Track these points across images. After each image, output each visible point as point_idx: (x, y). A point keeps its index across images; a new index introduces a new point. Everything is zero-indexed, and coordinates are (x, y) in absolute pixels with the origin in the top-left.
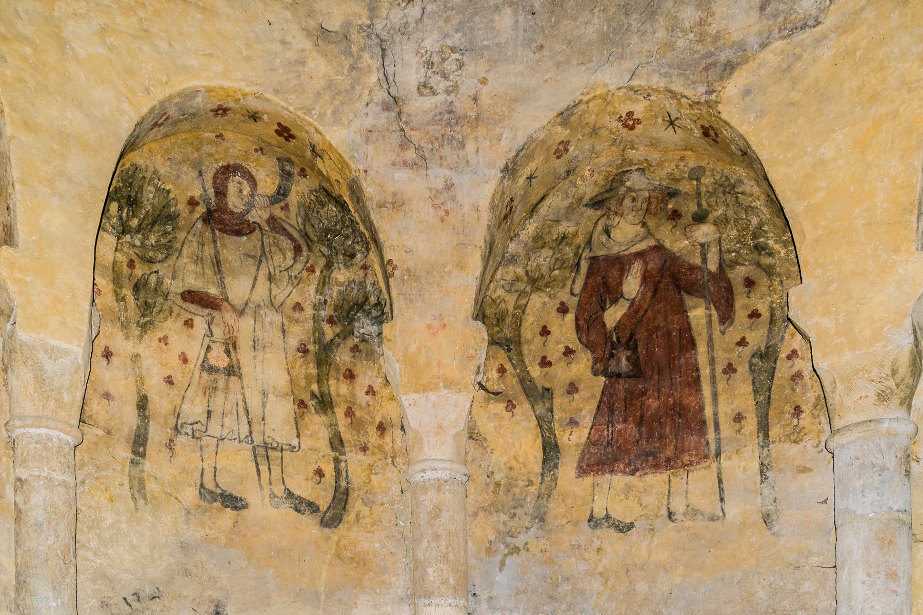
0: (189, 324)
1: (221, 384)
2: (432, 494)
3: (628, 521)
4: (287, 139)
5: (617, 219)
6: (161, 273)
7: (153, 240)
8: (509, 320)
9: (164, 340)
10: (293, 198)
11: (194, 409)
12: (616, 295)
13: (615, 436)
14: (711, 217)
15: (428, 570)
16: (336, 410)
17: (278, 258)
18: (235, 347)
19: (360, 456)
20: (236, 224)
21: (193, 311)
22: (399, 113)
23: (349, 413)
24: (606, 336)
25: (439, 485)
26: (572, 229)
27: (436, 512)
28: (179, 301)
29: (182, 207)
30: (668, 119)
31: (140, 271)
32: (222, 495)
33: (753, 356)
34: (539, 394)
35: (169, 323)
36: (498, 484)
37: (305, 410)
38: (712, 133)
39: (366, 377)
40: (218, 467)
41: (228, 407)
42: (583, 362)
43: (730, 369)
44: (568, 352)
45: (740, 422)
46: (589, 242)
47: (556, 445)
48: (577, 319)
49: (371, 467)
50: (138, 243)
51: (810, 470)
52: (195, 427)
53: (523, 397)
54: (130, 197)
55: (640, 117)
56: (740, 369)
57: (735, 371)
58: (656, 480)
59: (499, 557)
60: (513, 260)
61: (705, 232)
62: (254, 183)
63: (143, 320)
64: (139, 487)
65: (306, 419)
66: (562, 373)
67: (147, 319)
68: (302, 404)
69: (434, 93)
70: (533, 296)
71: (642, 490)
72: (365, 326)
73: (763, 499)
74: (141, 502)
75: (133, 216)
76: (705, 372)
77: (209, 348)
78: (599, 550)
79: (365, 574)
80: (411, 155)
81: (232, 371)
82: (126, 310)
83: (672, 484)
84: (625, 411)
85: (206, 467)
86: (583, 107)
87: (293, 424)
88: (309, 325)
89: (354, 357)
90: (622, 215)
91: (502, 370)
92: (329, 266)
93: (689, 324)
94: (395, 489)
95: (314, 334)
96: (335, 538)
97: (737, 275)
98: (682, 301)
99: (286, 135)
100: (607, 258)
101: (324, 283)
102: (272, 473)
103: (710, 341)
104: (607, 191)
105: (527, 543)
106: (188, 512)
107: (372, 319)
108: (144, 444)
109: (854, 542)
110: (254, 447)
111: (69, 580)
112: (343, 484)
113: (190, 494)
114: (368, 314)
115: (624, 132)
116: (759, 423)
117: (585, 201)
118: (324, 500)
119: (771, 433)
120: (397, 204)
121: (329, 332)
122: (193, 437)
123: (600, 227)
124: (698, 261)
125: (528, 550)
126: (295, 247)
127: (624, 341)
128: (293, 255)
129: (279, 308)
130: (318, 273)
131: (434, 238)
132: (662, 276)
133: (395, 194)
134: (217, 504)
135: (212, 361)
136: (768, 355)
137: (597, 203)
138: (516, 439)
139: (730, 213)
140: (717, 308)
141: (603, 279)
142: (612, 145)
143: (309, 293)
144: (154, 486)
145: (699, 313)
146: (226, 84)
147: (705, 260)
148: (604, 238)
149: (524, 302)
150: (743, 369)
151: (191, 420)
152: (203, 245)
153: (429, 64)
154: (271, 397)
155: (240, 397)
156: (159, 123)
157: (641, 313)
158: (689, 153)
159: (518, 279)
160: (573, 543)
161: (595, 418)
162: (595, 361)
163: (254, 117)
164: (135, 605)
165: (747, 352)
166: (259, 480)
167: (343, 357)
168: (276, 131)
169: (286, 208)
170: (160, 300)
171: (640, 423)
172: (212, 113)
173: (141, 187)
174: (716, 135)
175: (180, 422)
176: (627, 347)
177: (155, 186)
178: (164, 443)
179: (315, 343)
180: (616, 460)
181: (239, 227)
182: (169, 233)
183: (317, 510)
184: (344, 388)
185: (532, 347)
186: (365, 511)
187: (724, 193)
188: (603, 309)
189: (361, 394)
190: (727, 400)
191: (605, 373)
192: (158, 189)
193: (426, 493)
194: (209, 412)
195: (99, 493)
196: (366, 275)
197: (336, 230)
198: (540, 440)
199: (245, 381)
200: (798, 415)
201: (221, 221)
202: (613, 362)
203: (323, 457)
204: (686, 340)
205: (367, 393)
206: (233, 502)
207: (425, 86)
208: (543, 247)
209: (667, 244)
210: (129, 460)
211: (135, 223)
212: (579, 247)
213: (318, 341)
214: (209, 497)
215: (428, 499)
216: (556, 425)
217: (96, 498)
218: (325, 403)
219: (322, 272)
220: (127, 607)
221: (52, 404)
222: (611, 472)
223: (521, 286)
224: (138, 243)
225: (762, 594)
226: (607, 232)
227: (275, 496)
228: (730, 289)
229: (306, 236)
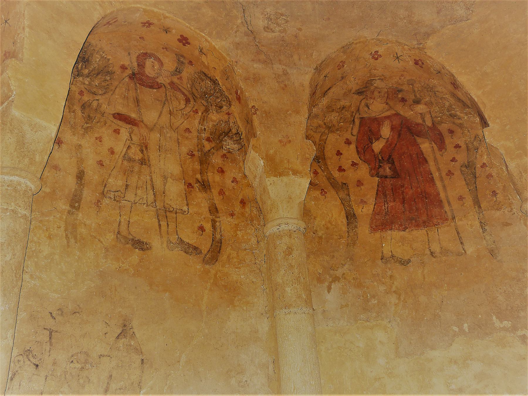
0: (117, 131)
1: (136, 169)
2: (286, 240)
3: (406, 258)
4: (184, 45)
5: (372, 101)
6: (100, 101)
9: (100, 139)
10: (185, 74)
13: (389, 209)
15: (287, 289)
16: (213, 190)
17: (175, 103)
18: (146, 147)
19: (230, 219)
20: (150, 83)
21: (120, 125)
22: (255, 38)
23: (221, 192)
24: (375, 157)
25: (290, 234)
26: (348, 104)
27: (289, 251)
28: (112, 118)
29: (117, 70)
30: (396, 55)
31: (86, 98)
32: (133, 240)
33: (461, 166)
35: (103, 129)
36: (321, 238)
37: (192, 189)
38: (420, 63)
39: (231, 173)
40: (131, 221)
41: (140, 183)
42: (364, 171)
43: (450, 173)
44: (354, 164)
45: (462, 200)
47: (354, 214)
49: (237, 225)
50: (87, 83)
51: (511, 224)
52: (116, 193)
53: (330, 187)
54: (84, 58)
55: (381, 54)
56: (455, 173)
57: (453, 174)
58: (420, 234)
59: (327, 284)
61: (421, 108)
62: (161, 64)
63: (86, 125)
64: (72, 230)
65: (193, 195)
67: (88, 125)
68: (190, 185)
70: (330, 135)
71: (411, 240)
72: (230, 144)
73: (487, 241)
74: (72, 241)
75: (85, 68)
76: (436, 175)
77: (129, 147)
78: (391, 277)
79: (235, 297)
81: (143, 162)
82: (75, 118)
83: (429, 236)
84: (393, 195)
85: (122, 220)
86: (354, 46)
87: (184, 196)
88: (195, 141)
89: (224, 160)
90: (374, 99)
92: (207, 110)
93: (421, 151)
94: (254, 240)
95: (198, 146)
96: (213, 272)
97: (444, 128)
98: (415, 140)
99: (184, 42)
100: (369, 118)
101: (203, 119)
102: (170, 227)
103: (435, 160)
104: (364, 88)
105: (344, 274)
106: (107, 250)
107: (234, 141)
108: (79, 201)
110: (157, 210)
111: (16, 290)
112: (218, 236)
113: (110, 237)
115: (372, 61)
116: (474, 200)
117: (352, 92)
118: (205, 246)
119: (482, 206)
121: (208, 146)
122: (115, 200)
123: (363, 103)
124: (420, 121)
125: (345, 278)
126: (186, 99)
127: (386, 159)
128: (185, 103)
129: (176, 130)
130: (200, 114)
132: (402, 128)
133: (254, 74)
134: (129, 246)
136: (469, 166)
137: (359, 93)
138: (331, 211)
139: (433, 100)
140: (435, 143)
141: (369, 130)
142: (364, 67)
144: (83, 230)
145: (426, 146)
146: (156, 10)
147: (424, 121)
148: (366, 109)
149: (325, 138)
150: (457, 173)
151: (114, 189)
152: (129, 90)
155: (148, 178)
156: (108, 22)
157: (393, 146)
158: (405, 73)
159: (320, 126)
160: (374, 273)
161: (376, 199)
162: (371, 170)
163: (167, 30)
164: (59, 318)
165: (458, 164)
166: (160, 231)
167: (216, 160)
168: (179, 40)
169: (180, 78)
170: (99, 116)
171: (403, 202)
172: (142, 25)
173: (92, 54)
174: (423, 63)
175: (106, 189)
176: (388, 162)
177: (101, 55)
178: (93, 202)
179: (198, 151)
180: (392, 223)
181: (154, 85)
182: (108, 81)
183: (201, 252)
184: (218, 178)
185: (332, 162)
186: (234, 254)
187: (428, 91)
188: (372, 143)
190: (452, 190)
191: (377, 175)
193: (281, 239)
194: (127, 186)
195: (41, 231)
196: (229, 118)
197: (211, 93)
198: (343, 213)
199: (153, 169)
200: (495, 196)
201: (141, 80)
202: (381, 170)
203: (204, 218)
205: (233, 182)
206: (140, 245)
207: (267, 28)
208: (333, 111)
209: (402, 113)
210: (66, 211)
211: (86, 71)
212: (353, 112)
213: (201, 150)
214: (123, 241)
215: (282, 244)
216: (353, 203)
217: (38, 235)
219: (202, 113)
220: (52, 320)
221: (27, 160)
222: (391, 229)
224: (87, 83)
227: (171, 242)
228: (440, 134)
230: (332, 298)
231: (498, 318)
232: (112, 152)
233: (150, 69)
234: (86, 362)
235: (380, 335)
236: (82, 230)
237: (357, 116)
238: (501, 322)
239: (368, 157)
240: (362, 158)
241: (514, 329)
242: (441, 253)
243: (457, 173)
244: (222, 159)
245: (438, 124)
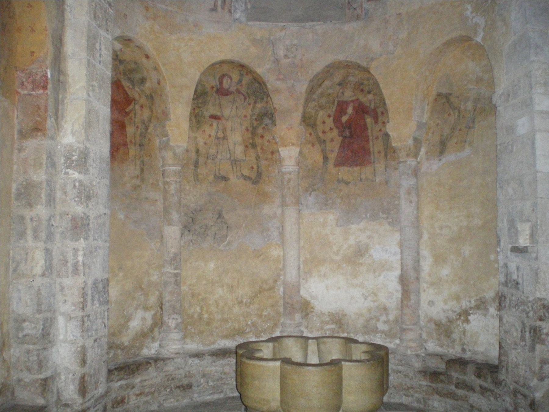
0: (211, 125)
1: (221, 143)
3: (349, 181)
7: (200, 101)
8: (313, 118)
9: (204, 131)
10: (244, 82)
11: (213, 151)
14: (372, 92)
19: (266, 162)
23: (262, 149)
24: (342, 125)
25: (290, 173)
27: (289, 181)
29: (209, 89)
34: (322, 142)
36: (309, 169)
42: (335, 132)
44: (331, 129)
46: (337, 96)
58: (356, 169)
59: (309, 192)
60: (314, 100)
61: (370, 97)
62: (231, 78)
66: (329, 135)
68: (247, 147)
69: (289, 58)
72: (267, 121)
74: (197, 182)
76: (371, 138)
80: (282, 76)
81: (225, 138)
91: (310, 134)
94: (277, 171)
97: (379, 110)
101: (254, 108)
106: (211, 183)
109: (402, 193)
112: (260, 171)
113: (211, 178)
114: (268, 117)
118: (254, 176)
120: (278, 91)
121: (255, 123)
124: (368, 105)
131: (288, 98)
135: (219, 136)
137: (340, 84)
138: (315, 156)
141: (341, 108)
143: (249, 112)
145: (369, 120)
147: (370, 104)
150: (380, 138)
153: (287, 49)
154: (237, 145)
164: (195, 213)
165: (382, 133)
167: (260, 131)
169: (241, 86)
176: (349, 129)
183: (252, 179)
185: (320, 127)
189: (265, 142)
190: (376, 147)
191: (342, 136)
192: (202, 85)
194: (217, 152)
204: (365, 128)
206: (225, 179)
215: (287, 177)
216: (327, 151)
218: (254, 146)
223: (317, 108)
225: (385, 204)
226: (343, 93)
228: (377, 114)
229: (248, 93)
230: (311, 199)
232: (210, 136)
233: (226, 83)
234: (206, 228)
235: (331, 217)
236: (201, 176)
237: (337, 99)
241: (387, 218)
243: (380, 138)
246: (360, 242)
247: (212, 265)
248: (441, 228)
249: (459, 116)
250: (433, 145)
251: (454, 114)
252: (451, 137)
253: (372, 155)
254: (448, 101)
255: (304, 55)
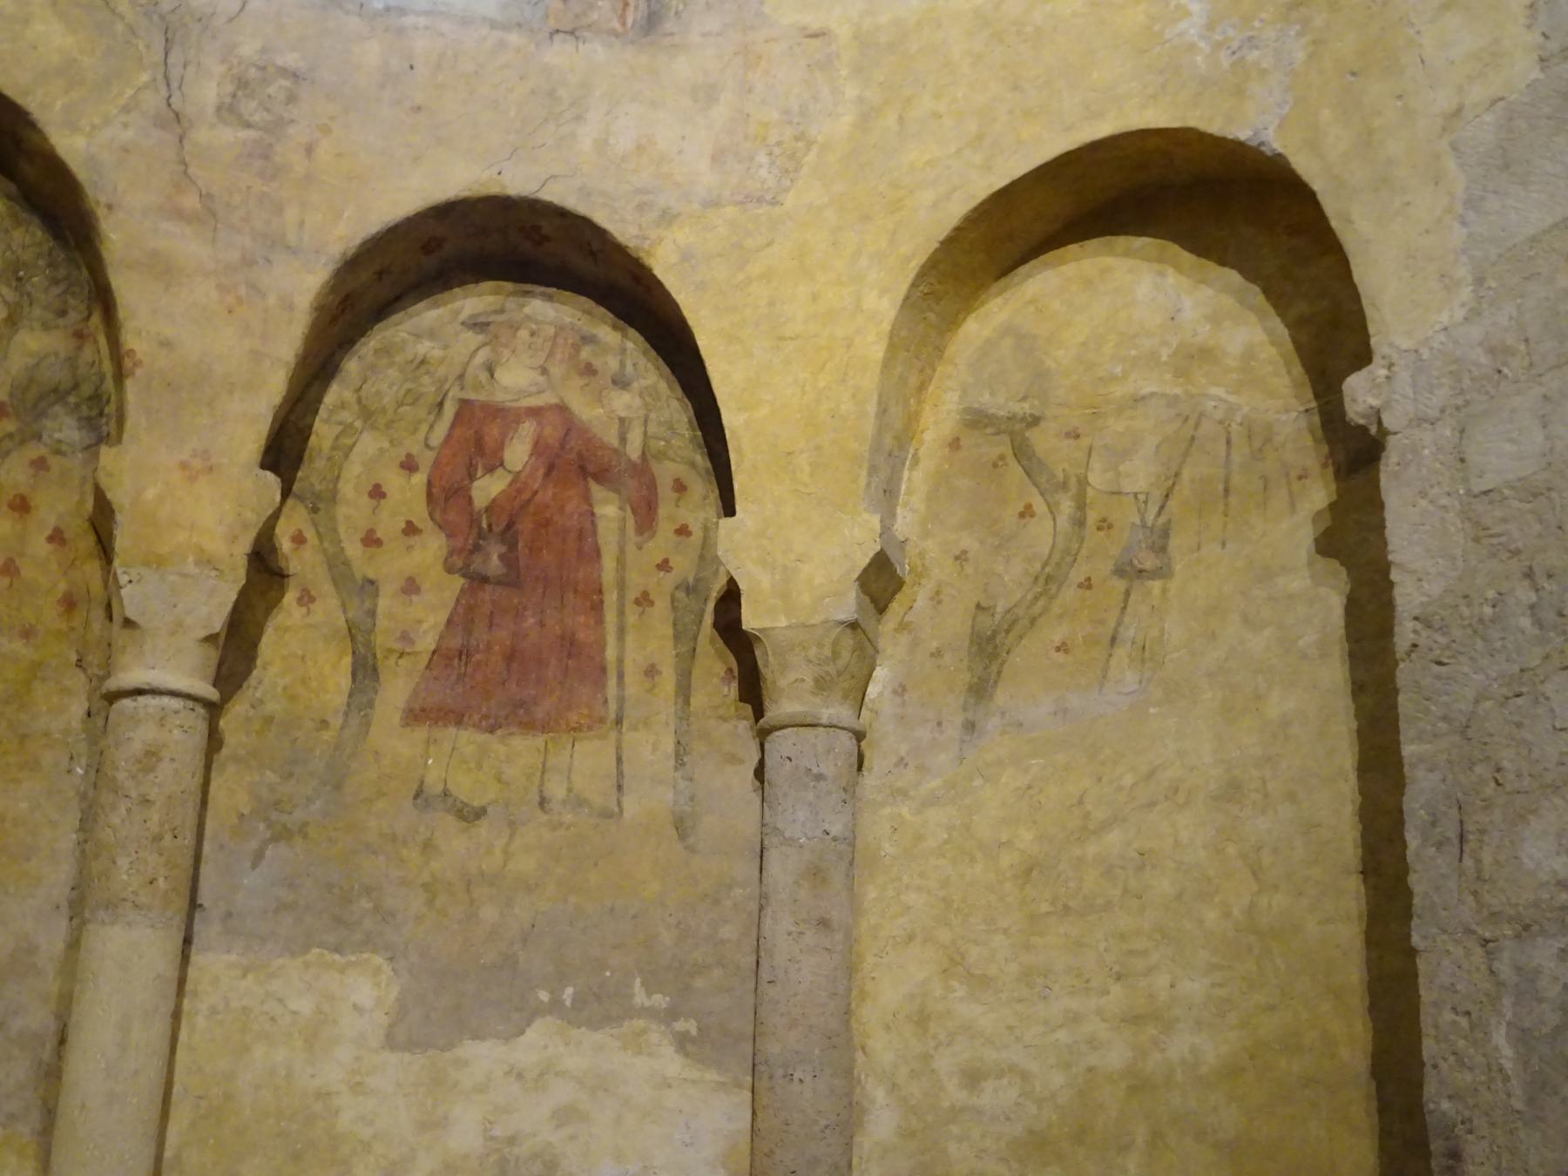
12: (495, 464)
27: (151, 757)
36: (269, 720)
42: (432, 547)
44: (411, 529)
46: (461, 377)
48: (430, 484)
56: (657, 603)
57: (652, 603)
59: (254, 844)
76: (611, 598)
80: (191, 202)
120: (163, 270)
124: (615, 442)
145: (609, 510)
147: (623, 439)
148: (483, 376)
149: (349, 441)
150: (661, 606)
176: (503, 541)
198: (347, 660)
226: (490, 369)
228: (652, 486)
231: (643, 984)
238: (649, 994)
239: (452, 516)
240: (437, 516)
241: (672, 1014)
242: (564, 802)
244: (32, 471)
245: (654, 457)
246: (512, 1141)
247: (1448, 432)
248: (973, 1077)
249: (1080, 523)
250: (937, 654)
251: (1053, 510)
252: (1033, 621)
253: (612, 682)
254: (1022, 452)
255: (326, 130)
